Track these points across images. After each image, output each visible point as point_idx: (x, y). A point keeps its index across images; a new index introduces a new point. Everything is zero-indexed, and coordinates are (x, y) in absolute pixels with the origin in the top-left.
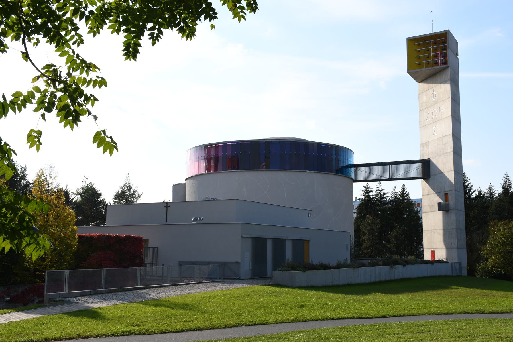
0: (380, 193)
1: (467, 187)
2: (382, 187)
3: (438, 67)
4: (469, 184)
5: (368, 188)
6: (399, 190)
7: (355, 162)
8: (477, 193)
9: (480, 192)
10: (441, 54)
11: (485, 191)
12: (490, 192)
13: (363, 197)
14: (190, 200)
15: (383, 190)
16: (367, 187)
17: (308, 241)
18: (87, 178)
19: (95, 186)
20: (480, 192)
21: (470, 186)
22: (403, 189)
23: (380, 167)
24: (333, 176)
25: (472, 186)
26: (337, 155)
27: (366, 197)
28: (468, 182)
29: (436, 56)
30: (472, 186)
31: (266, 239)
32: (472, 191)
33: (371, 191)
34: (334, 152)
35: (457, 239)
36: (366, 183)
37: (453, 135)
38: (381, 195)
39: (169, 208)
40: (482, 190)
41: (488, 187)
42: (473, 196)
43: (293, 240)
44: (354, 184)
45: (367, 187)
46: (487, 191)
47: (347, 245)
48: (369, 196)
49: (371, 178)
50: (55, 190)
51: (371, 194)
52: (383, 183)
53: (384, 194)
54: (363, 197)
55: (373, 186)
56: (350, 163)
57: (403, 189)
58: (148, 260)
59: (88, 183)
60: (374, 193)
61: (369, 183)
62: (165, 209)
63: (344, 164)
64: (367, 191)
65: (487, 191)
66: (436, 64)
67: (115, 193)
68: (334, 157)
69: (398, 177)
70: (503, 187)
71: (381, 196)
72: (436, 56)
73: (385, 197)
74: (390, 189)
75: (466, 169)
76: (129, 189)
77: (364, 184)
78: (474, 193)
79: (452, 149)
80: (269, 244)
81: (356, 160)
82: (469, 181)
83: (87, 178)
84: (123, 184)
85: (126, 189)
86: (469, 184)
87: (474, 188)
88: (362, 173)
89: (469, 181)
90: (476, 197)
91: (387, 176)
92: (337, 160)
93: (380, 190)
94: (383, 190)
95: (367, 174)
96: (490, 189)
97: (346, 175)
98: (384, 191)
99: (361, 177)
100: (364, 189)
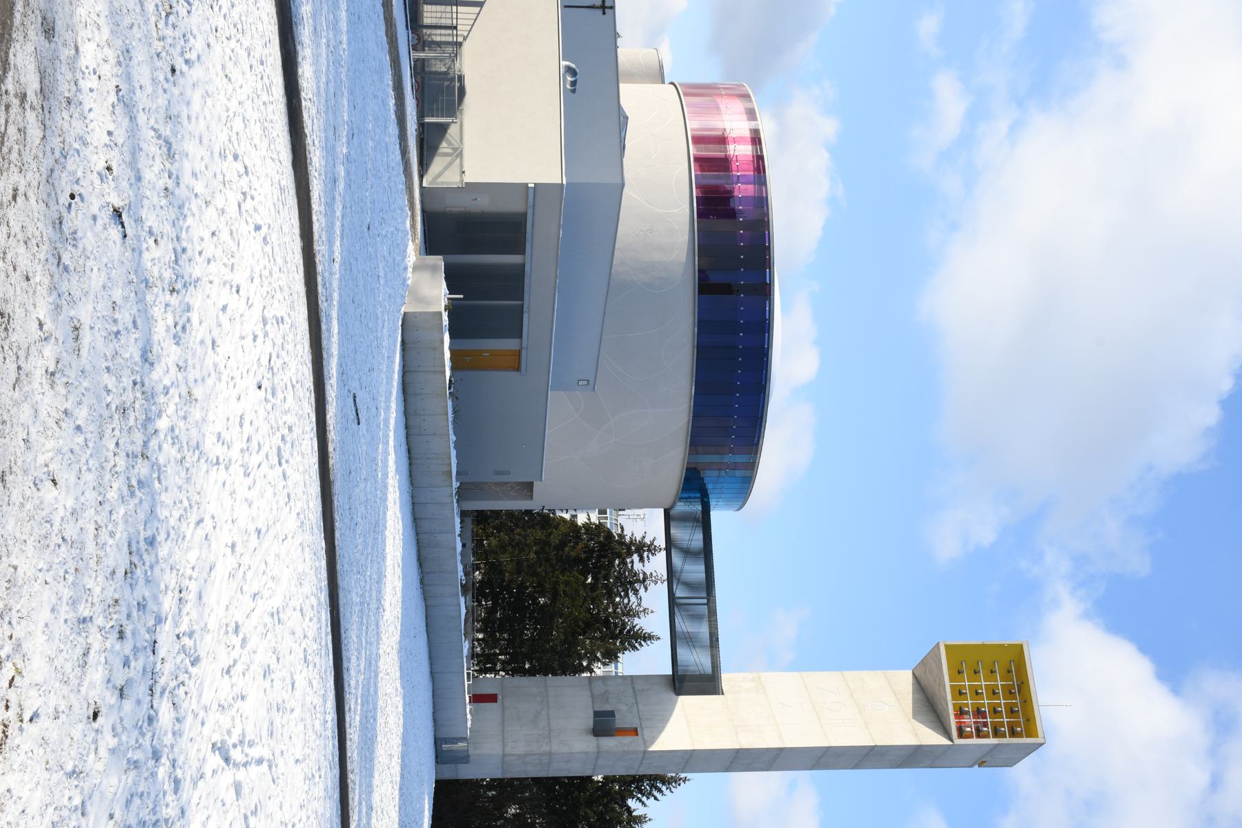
0: (638, 581)
1: (653, 786)
2: (652, 587)
3: (952, 717)
4: (660, 791)
5: (649, 550)
7: (714, 514)
10: (985, 724)
13: (628, 539)
15: (646, 589)
16: (652, 549)
17: (518, 369)
21: (655, 793)
22: (648, 637)
23: (703, 576)
24: (681, 457)
25: (656, 799)
26: (735, 466)
27: (628, 546)
28: (664, 788)
29: (979, 713)
30: (656, 799)
31: (521, 251)
33: (642, 560)
34: (740, 459)
35: (526, 755)
36: (663, 546)
37: (781, 750)
38: (631, 583)
39: (600, 11)
42: (631, 803)
43: (523, 266)
45: (652, 549)
47: (508, 473)
48: (630, 554)
49: (673, 551)
51: (636, 557)
52: (664, 587)
53: (636, 592)
54: (628, 539)
55: (656, 564)
56: (713, 503)
57: (648, 637)
58: (492, 681)
60: (638, 566)
61: (663, 553)
62: (598, 2)
63: (709, 486)
64: (642, 548)
66: (961, 713)
68: (729, 458)
69: (678, 620)
71: (631, 582)
72: (979, 713)
74: (652, 607)
75: (698, 784)
77: (661, 542)
79: (745, 745)
80: (509, 344)
81: (719, 517)
86: (660, 791)
88: (689, 536)
91: (679, 592)
92: (720, 467)
93: (644, 580)
94: (646, 589)
95: (685, 544)
97: (681, 499)
98: (642, 591)
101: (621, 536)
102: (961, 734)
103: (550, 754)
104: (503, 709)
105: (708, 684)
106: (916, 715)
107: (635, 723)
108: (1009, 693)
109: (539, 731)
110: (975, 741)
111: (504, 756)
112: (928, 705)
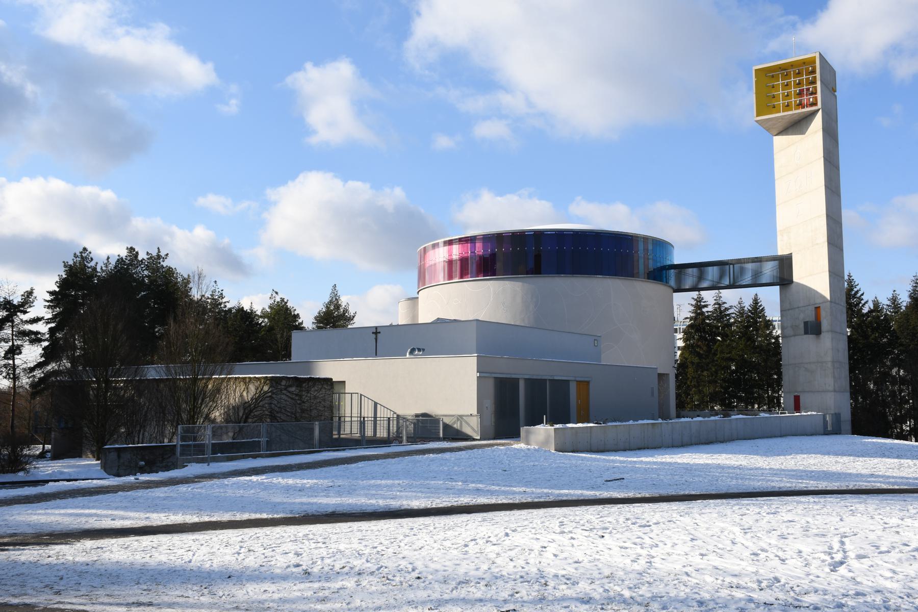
0: (719, 308)
2: (723, 300)
4: (857, 292)
6: (748, 304)
7: (677, 261)
8: (870, 305)
9: (876, 304)
11: (884, 301)
12: (893, 303)
14: (517, 323)
16: (699, 300)
18: (277, 293)
19: (289, 305)
20: (876, 304)
21: (859, 295)
22: (756, 301)
23: (715, 268)
24: (641, 283)
27: (697, 314)
29: (800, 94)
32: (863, 302)
33: (706, 306)
34: (641, 246)
35: (834, 377)
36: (697, 293)
37: (828, 216)
38: (721, 312)
40: (880, 301)
41: (890, 296)
42: (865, 310)
43: (526, 379)
44: (675, 294)
45: (699, 300)
46: (889, 303)
48: (703, 313)
50: (234, 311)
51: (705, 310)
53: (727, 309)
55: (709, 297)
56: (669, 263)
57: (756, 301)
59: (278, 299)
60: (710, 309)
62: (374, 336)
64: (699, 305)
65: (889, 303)
67: (316, 314)
70: (910, 296)
71: (721, 312)
72: (800, 94)
73: (729, 315)
74: (735, 299)
76: (338, 307)
77: (695, 294)
78: (867, 305)
80: (573, 388)
82: (858, 288)
83: (277, 293)
84: (327, 300)
85: (332, 308)
86: (857, 292)
87: (865, 298)
88: (690, 279)
89: (858, 288)
90: (871, 311)
91: (726, 282)
95: (695, 279)
96: (894, 300)
98: (726, 306)
99: (688, 283)
100: (694, 303)
101: (691, 319)
102: (815, 104)
103: (833, 362)
104: (804, 392)
105: (785, 263)
106: (803, 133)
107: (812, 308)
108: (787, 76)
109: (819, 369)
110: (819, 95)
111: (835, 391)
112: (797, 126)
